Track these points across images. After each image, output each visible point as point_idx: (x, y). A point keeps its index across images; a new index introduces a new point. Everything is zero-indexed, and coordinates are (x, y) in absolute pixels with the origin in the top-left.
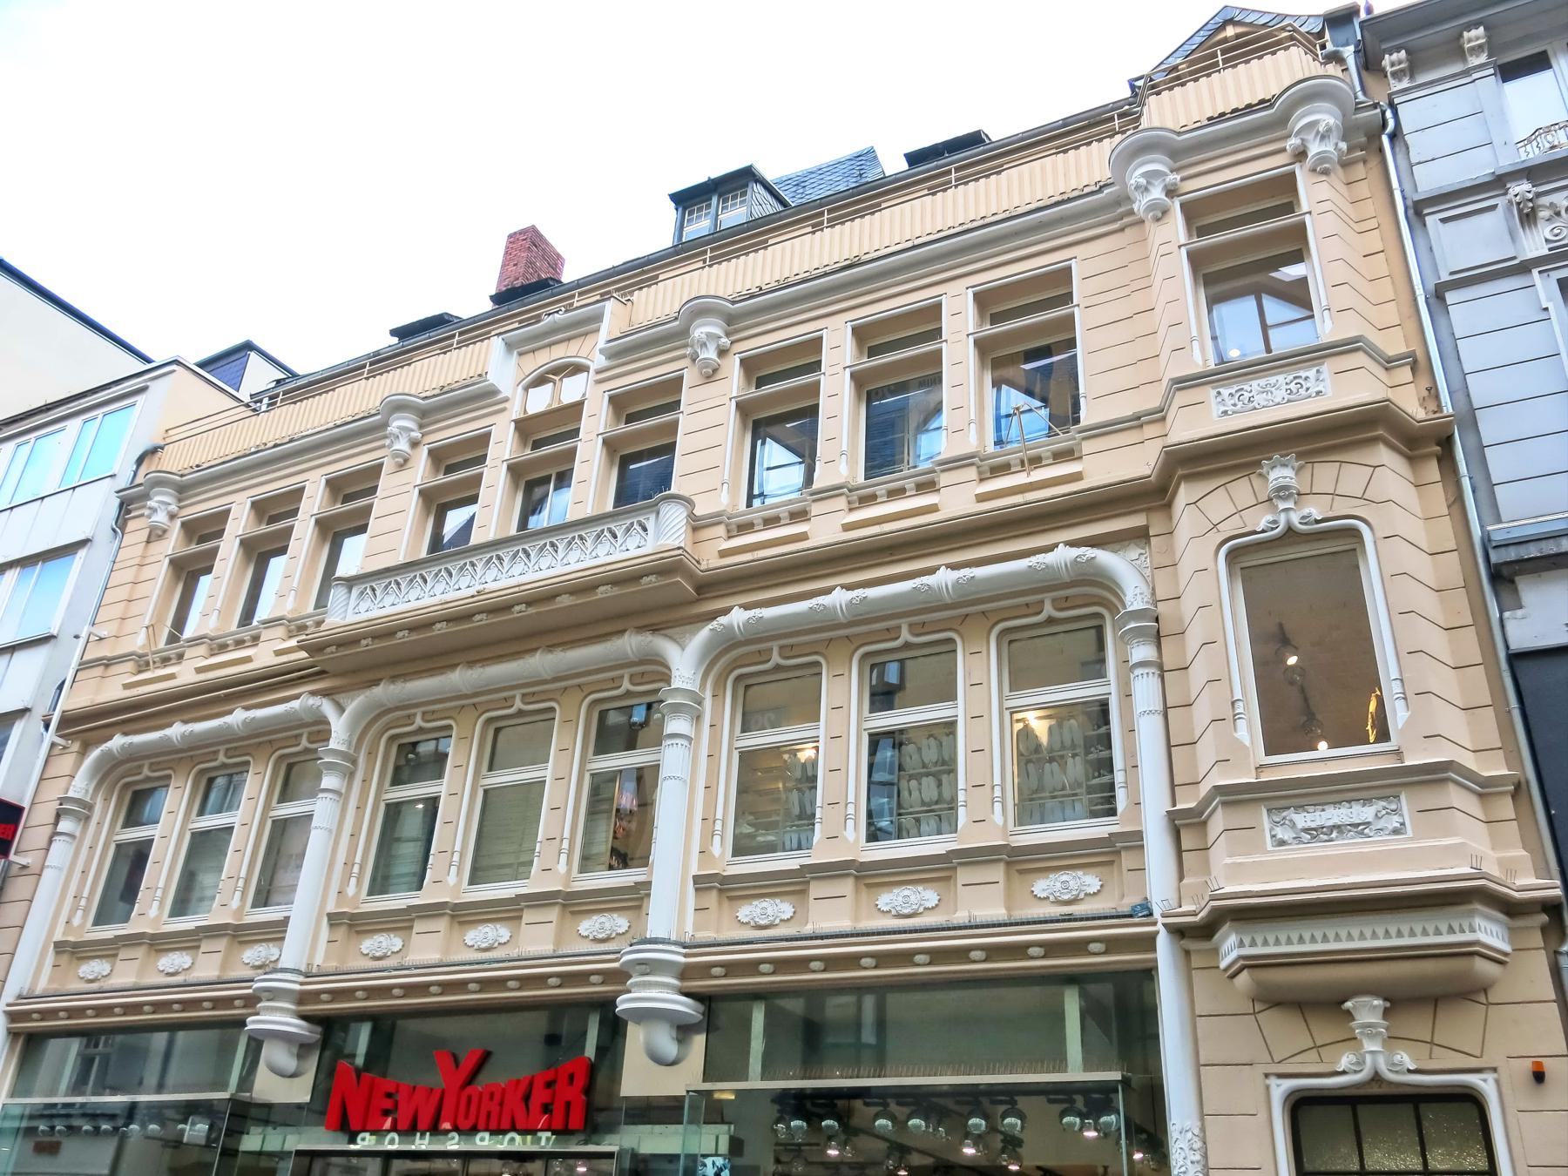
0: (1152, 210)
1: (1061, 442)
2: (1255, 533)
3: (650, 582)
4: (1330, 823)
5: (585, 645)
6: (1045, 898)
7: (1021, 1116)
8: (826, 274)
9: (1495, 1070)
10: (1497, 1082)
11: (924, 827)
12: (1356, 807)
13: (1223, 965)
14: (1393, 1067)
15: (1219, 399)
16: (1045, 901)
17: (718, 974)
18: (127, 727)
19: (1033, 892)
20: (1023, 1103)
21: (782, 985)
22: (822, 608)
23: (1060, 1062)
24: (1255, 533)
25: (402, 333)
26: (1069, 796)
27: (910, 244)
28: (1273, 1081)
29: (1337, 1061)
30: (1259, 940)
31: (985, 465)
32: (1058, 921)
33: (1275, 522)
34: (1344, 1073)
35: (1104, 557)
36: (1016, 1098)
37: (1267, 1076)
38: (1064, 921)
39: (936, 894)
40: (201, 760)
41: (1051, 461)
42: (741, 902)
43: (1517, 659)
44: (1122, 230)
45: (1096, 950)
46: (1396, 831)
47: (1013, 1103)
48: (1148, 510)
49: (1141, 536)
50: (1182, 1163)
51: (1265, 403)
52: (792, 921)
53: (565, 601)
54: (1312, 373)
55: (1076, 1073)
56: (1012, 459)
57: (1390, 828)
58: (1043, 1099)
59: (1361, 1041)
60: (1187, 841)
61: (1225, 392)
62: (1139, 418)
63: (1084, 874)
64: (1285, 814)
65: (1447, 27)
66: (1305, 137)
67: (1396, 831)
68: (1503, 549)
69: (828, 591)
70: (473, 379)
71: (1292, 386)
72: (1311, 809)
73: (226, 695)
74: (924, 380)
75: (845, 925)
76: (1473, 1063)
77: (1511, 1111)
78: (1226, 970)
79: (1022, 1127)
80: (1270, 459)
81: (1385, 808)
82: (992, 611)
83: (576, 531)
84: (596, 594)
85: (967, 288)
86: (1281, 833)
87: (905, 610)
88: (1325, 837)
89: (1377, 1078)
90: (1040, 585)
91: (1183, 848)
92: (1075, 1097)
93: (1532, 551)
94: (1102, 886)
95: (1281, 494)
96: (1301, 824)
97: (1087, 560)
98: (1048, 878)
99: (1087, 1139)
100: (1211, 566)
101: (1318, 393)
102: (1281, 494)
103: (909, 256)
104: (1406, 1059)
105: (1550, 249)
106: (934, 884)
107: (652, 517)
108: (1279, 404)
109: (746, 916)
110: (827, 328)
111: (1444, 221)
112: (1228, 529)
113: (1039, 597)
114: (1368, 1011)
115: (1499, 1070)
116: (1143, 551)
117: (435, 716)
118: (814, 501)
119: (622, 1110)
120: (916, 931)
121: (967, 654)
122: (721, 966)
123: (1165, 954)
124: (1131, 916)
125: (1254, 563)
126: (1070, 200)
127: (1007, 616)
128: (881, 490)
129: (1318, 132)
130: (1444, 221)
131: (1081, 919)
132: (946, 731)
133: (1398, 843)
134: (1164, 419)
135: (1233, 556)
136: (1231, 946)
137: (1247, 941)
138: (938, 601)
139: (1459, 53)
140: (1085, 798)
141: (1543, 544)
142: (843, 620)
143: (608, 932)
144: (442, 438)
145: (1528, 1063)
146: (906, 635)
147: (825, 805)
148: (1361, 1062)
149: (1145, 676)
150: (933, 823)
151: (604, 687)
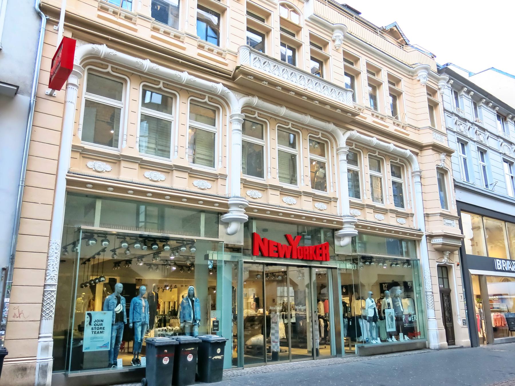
2: (439, 165)
3: (349, 115)
5: (322, 121)
6: (91, 168)
8: (366, 43)
13: (432, 242)
17: (131, 193)
18: (111, 44)
23: (93, 224)
24: (439, 165)
29: (442, 260)
31: (101, 4)
44: (409, 78)
47: (106, 237)
52: (110, 173)
53: (328, 107)
63: (161, 174)
73: (182, 63)
82: (278, 119)
83: (278, 64)
84: (289, 93)
89: (445, 264)
98: (93, 162)
99: (385, 269)
106: (112, 164)
107: (345, 93)
109: (148, 175)
111: (447, 116)
119: (241, 249)
121: (132, 88)
122: (92, 184)
123: (424, 238)
127: (281, 123)
128: (207, 47)
131: (175, 190)
134: (419, 130)
136: (436, 241)
142: (102, 57)
143: (158, 179)
146: (206, 100)
147: (305, 176)
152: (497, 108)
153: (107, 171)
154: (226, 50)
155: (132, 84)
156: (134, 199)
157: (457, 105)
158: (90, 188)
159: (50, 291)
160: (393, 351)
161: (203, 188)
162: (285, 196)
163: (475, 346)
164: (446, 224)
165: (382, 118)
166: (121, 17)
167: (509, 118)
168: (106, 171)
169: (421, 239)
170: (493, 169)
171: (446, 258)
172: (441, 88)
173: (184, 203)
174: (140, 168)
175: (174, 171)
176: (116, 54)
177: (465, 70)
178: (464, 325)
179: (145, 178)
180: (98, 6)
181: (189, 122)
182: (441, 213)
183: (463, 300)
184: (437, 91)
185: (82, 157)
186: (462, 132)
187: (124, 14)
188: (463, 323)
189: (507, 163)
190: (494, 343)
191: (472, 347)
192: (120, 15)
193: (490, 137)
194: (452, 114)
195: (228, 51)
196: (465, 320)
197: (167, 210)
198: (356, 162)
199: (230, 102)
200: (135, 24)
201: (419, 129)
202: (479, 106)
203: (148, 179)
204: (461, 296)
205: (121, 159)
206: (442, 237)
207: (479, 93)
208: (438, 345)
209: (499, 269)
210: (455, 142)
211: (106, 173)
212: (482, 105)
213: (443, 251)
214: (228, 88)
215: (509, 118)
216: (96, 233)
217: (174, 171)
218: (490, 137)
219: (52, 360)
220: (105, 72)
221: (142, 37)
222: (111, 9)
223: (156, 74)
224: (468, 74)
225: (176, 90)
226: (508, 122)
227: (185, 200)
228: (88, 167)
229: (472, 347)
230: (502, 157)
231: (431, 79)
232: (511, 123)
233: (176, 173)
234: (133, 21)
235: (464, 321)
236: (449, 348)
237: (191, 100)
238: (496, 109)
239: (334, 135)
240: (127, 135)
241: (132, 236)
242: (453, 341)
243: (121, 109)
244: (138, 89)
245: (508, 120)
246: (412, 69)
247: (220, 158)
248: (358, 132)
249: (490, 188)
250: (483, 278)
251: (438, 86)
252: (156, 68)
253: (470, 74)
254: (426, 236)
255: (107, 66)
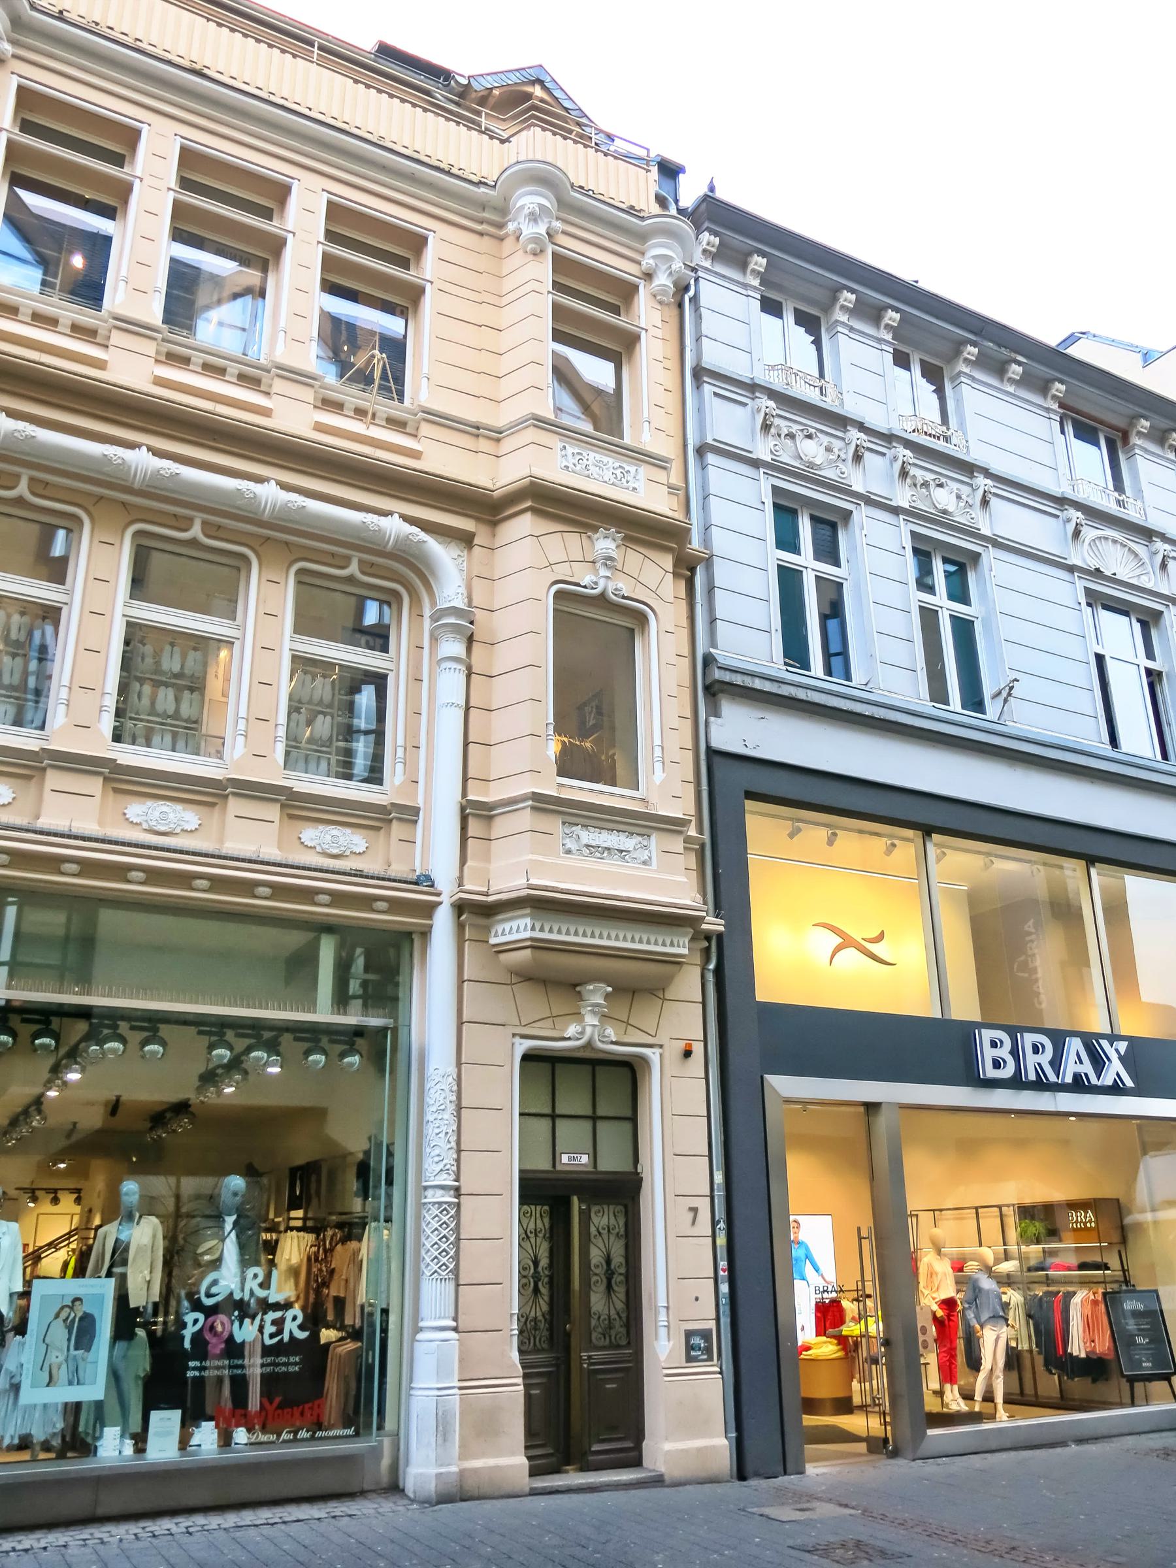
0: (536, 243)
1: (52, 306)
2: (578, 585)
4: (605, 845)
6: (311, 847)
7: (163, 1043)
9: (661, 1046)
10: (661, 1055)
11: (156, 739)
12: (622, 836)
13: (493, 941)
14: (603, 1038)
15: (563, 453)
16: (137, 827)
19: (125, 814)
20: (165, 1030)
21: (156, 898)
22: (119, 461)
23: (312, 1006)
24: (578, 585)
25: (385, 51)
26: (141, 720)
27: (281, 102)
28: (517, 1040)
29: (565, 1030)
30: (547, 928)
31: (165, 347)
32: (350, 875)
33: (596, 583)
34: (569, 1039)
35: (434, 546)
36: (51, 1018)
37: (514, 1035)
38: (355, 875)
39: (197, 817)
40: (310, 557)
41: (29, 320)
42: (308, 824)
43: (712, 753)
44: (481, 234)
45: (323, 902)
46: (644, 863)
48: (477, 519)
49: (466, 540)
50: (442, 1102)
51: (597, 477)
52: (10, 808)
54: (632, 469)
55: (323, 1014)
56: (232, 367)
57: (643, 859)
58: (192, 1030)
59: (583, 1015)
60: (474, 827)
61: (570, 450)
62: (478, 428)
63: (184, 809)
64: (574, 828)
65: (737, 237)
66: (660, 265)
67: (644, 863)
68: (723, 671)
69: (132, 446)
70: (138, 43)
71: (618, 472)
72: (592, 829)
74: (223, 250)
75: (91, 827)
76: (650, 1040)
77: (668, 1074)
78: (494, 946)
79: (123, 1052)
80: (606, 529)
81: (640, 843)
85: (323, 190)
86: (570, 844)
87: (217, 507)
88: (599, 855)
89: (589, 1045)
90: (234, 511)
91: (470, 834)
92: (52, 1018)
93: (738, 680)
94: (14, 799)
95: (608, 563)
96: (585, 840)
97: (419, 542)
100: (544, 599)
101: (634, 489)
102: (608, 563)
103: (271, 112)
104: (611, 1033)
105: (772, 459)
106: (12, 780)
108: (605, 482)
110: (149, 125)
111: (716, 394)
112: (562, 572)
113: (17, 469)
114: (596, 994)
115: (664, 1047)
116: (462, 554)
117: (220, 534)
118: (279, 376)
120: (169, 850)
121: (264, 580)
123: (443, 923)
124: (416, 883)
125: (566, 609)
126: (449, 173)
129: (670, 267)
130: (716, 394)
132: (192, 644)
133: (645, 872)
134: (498, 440)
135: (559, 595)
137: (538, 927)
138: (123, 480)
139: (743, 266)
140: (334, 759)
141: (810, 693)
143: (343, 849)
144: (375, 207)
145: (682, 1044)
146: (196, 531)
147: (252, 720)
148: (582, 1033)
149: (457, 671)
150: (168, 738)
151: (155, 520)
152: (1059, 388)
153: (186, 831)
154: (416, 412)
155: (263, 569)
156: (238, 907)
157: (1119, 486)
158: (266, 898)
159: (446, 1203)
160: (101, 1511)
161: (335, 851)
162: (142, 799)
163: (758, 1475)
164: (586, 851)
165: (244, 379)
166: (377, 421)
167: (1139, 433)
168: (182, 830)
169: (431, 926)
170: (1006, 628)
171: (591, 1020)
172: (655, 271)
173: (200, 895)
174: (286, 818)
175: (231, 799)
176: (33, 434)
177: (1132, 345)
178: (690, 1359)
179: (305, 849)
180: (157, 353)
181: (288, 642)
182: (536, 797)
183: (704, 1224)
184: (635, 288)
185: (111, 792)
186: (812, 465)
187: (351, 402)
188: (689, 1347)
189: (1126, 613)
190: (920, 1453)
191: (742, 1476)
192: (374, 415)
193: (995, 495)
194: (890, 443)
195: (278, 368)
196: (705, 1335)
197: (108, 918)
198: (379, 641)
199: (433, 573)
200: (268, 394)
201: (497, 435)
202: (953, 379)
203: (313, 850)
204: (694, 1210)
205: (229, 790)
206: (528, 911)
207: (937, 317)
208: (438, 1476)
209: (991, 1073)
210: (760, 506)
211: (353, 857)
212: (967, 370)
213: (575, 985)
214: (423, 529)
215: (1139, 433)
216: (287, 1030)
217: (231, 799)
218: (995, 495)
219: (1074, 1354)
220: (11, 500)
221: (133, 386)
222: (233, 369)
223: (28, 454)
224: (1139, 357)
225: (80, 502)
226: (1137, 451)
227: (204, 883)
228: (302, 843)
229: (742, 1476)
230: (1080, 585)
231: (601, 236)
232: (1159, 456)
233: (235, 806)
234: (98, 337)
235: (696, 1341)
236: (534, 1492)
237: (300, 572)
238: (1054, 392)
239: (420, 566)
240: (70, 688)
241: (137, 1019)
242: (629, 1444)
243: (60, 609)
244: (283, 583)
245: (1135, 440)
246: (483, 189)
247: (242, 725)
248: (284, 486)
249: (992, 709)
250: (882, 1122)
251: (639, 263)
252: (417, 538)
253: (1147, 358)
254: (460, 908)
255: (191, 520)
